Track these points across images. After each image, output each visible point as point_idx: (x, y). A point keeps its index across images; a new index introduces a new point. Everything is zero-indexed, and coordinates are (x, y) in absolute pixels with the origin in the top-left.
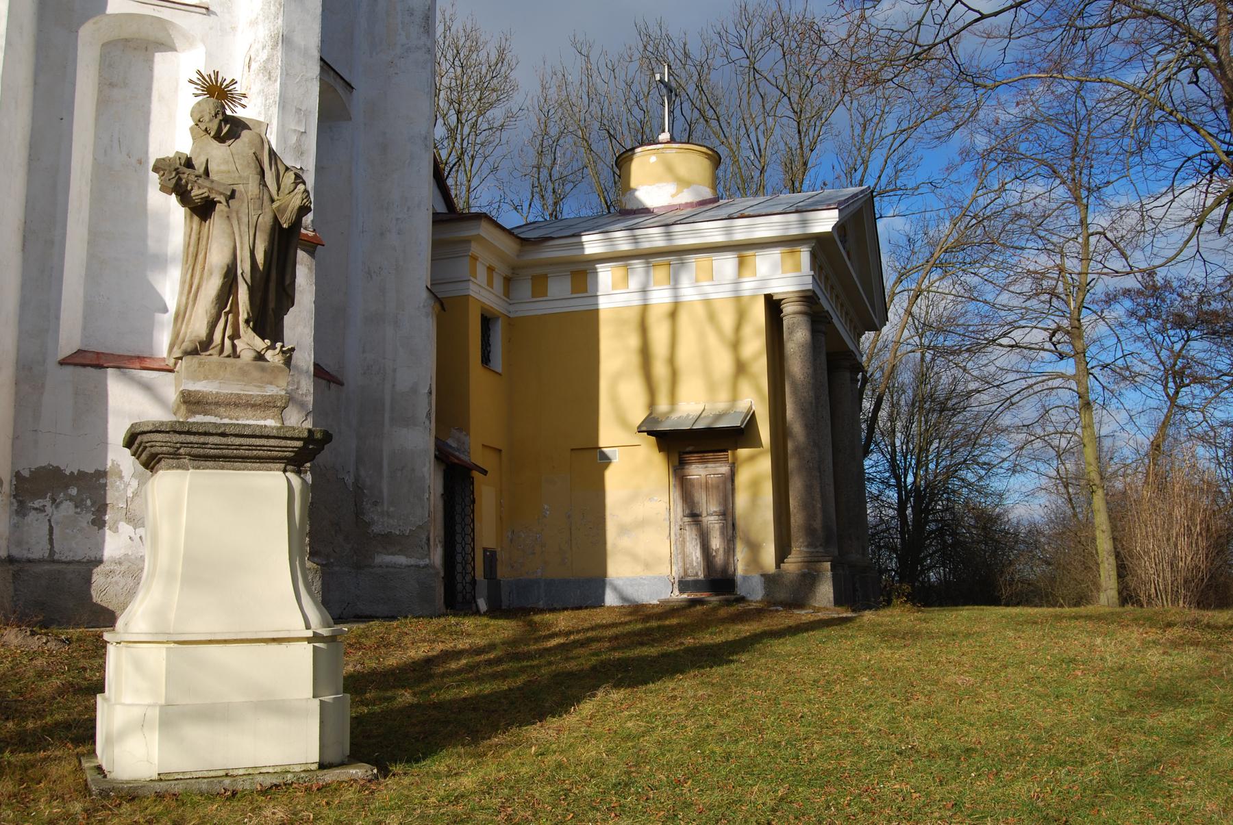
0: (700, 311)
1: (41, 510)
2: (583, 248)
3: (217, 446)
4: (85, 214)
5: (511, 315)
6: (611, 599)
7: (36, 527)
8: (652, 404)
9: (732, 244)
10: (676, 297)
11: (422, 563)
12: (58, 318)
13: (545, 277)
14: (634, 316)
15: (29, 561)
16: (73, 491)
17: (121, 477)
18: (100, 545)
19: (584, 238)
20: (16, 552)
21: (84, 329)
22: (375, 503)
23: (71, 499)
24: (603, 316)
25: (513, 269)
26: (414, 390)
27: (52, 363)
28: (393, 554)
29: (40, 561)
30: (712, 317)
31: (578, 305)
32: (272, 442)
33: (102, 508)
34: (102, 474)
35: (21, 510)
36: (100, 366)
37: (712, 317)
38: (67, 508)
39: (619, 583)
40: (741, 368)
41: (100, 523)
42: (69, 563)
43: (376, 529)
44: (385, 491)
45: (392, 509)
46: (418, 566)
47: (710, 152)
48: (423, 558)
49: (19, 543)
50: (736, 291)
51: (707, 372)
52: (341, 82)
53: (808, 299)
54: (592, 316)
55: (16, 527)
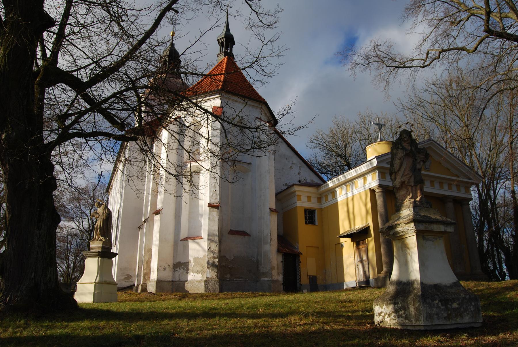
0: (358, 196)
1: (177, 271)
2: (329, 186)
3: (89, 255)
6: (345, 287)
7: (177, 273)
8: (350, 227)
9: (359, 175)
10: (353, 194)
11: (270, 279)
13: (327, 195)
14: (345, 201)
15: (176, 281)
16: (183, 266)
19: (328, 183)
20: (174, 280)
21: (188, 232)
22: (261, 265)
23: (182, 268)
24: (339, 203)
26: (267, 235)
27: (179, 240)
28: (264, 277)
29: (177, 281)
30: (361, 197)
31: (333, 202)
33: (188, 270)
34: (188, 262)
35: (174, 271)
36: (187, 240)
37: (361, 197)
38: (182, 270)
39: (348, 283)
40: (367, 212)
41: (187, 273)
43: (261, 271)
44: (263, 261)
46: (269, 280)
47: (387, 142)
48: (270, 278)
49: (174, 278)
50: (365, 188)
51: (361, 215)
52: (246, 164)
53: (380, 186)
54: (337, 203)
55: (173, 274)
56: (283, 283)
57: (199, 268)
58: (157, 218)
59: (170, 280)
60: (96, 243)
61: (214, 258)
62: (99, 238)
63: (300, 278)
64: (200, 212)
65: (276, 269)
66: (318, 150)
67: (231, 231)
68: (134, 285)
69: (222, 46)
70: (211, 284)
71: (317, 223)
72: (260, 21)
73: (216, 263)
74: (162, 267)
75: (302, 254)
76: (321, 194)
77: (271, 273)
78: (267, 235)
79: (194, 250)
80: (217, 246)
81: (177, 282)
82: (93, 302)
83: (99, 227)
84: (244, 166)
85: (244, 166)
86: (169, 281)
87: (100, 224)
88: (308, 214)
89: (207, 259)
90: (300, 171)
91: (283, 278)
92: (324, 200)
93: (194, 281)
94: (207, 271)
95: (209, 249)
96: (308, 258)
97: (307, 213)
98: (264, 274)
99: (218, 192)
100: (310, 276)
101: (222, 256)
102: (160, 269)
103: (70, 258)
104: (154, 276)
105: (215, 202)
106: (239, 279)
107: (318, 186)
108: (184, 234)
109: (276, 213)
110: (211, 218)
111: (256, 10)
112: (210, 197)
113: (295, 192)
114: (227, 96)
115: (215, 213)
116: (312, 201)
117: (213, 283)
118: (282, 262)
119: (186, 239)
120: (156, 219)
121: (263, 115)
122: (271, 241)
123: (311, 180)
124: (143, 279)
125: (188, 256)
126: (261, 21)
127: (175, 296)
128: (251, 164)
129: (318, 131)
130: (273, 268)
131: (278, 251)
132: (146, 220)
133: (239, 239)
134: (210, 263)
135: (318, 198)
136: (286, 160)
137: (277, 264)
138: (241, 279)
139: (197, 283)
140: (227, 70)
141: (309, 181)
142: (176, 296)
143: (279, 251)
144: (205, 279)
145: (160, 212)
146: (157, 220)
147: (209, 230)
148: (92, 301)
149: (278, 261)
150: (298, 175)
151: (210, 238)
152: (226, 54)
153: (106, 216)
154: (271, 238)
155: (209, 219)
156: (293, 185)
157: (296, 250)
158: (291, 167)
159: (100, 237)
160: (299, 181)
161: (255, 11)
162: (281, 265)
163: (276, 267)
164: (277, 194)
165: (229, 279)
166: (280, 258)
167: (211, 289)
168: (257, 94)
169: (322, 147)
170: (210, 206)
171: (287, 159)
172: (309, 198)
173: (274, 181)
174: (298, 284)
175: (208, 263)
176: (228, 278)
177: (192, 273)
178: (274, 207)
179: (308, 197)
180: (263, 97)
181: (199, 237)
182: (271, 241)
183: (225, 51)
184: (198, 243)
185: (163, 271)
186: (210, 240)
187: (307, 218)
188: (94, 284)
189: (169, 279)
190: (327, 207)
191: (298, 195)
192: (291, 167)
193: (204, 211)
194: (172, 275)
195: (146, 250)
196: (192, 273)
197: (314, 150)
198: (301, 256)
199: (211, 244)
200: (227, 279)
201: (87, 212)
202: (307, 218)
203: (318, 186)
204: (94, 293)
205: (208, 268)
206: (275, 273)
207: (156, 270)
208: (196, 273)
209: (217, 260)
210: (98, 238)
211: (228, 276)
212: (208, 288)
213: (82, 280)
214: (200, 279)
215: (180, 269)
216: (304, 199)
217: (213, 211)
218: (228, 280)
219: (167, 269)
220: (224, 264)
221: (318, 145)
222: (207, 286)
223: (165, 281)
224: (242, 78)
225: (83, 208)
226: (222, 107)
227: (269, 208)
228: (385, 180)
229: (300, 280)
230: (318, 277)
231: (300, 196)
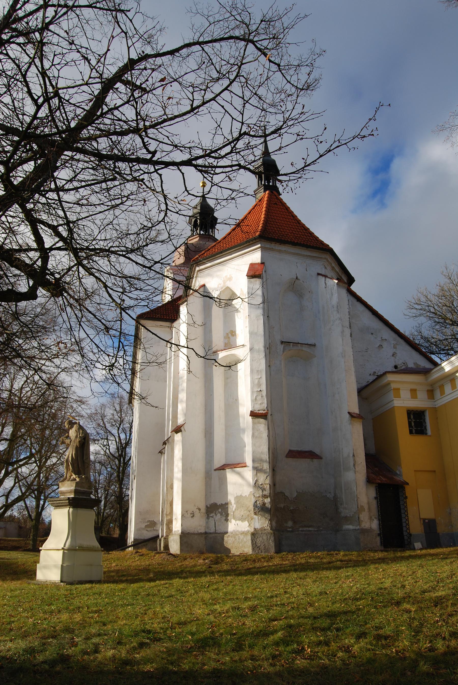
1: (212, 517)
2: (444, 370)
4: (223, 421)
5: (437, 406)
7: (211, 521)
12: (213, 456)
15: (210, 533)
16: (220, 510)
17: (231, 504)
18: (227, 527)
19: (443, 365)
20: (208, 531)
21: (226, 457)
22: (341, 504)
23: (219, 513)
25: (431, 385)
26: (349, 456)
28: (348, 525)
32: (64, 501)
33: (227, 515)
34: (227, 504)
35: (208, 517)
36: (224, 469)
41: (227, 520)
42: (219, 533)
43: (343, 515)
45: (346, 506)
46: (356, 530)
48: (357, 526)
52: (306, 346)
55: (207, 523)
56: (379, 532)
57: (243, 512)
58: (178, 437)
59: (203, 531)
60: (66, 485)
61: (265, 496)
62: (72, 477)
63: (408, 524)
64: (241, 425)
66: (422, 319)
67: (290, 451)
68: (158, 536)
69: (260, 179)
70: (261, 539)
71: (429, 432)
72: (288, 81)
73: (268, 505)
74: (189, 513)
75: (408, 484)
76: (432, 385)
77: (359, 518)
78: (349, 456)
79: (235, 484)
80: (268, 478)
81: (214, 535)
82: (61, 581)
83: (70, 459)
84: (304, 349)
85: (304, 349)
86: (201, 534)
87: (72, 455)
88: (414, 418)
89: (253, 500)
90: (394, 350)
91: (379, 525)
92: (437, 394)
93: (238, 533)
94: (255, 518)
95: (255, 484)
96: (418, 490)
97: (412, 417)
98: (347, 519)
99: (264, 393)
100: (424, 520)
101: (278, 492)
102: (186, 515)
103: (99, 491)
104: (177, 527)
105: (261, 408)
106: (307, 529)
107: (426, 372)
108: (218, 461)
109: (362, 420)
110: (256, 434)
111: (277, 62)
112: (252, 401)
113: (388, 384)
114: (268, 245)
115: (262, 425)
117: (265, 537)
118: (376, 498)
119: (223, 468)
120: (177, 439)
121: (329, 268)
122: (354, 465)
123: (414, 364)
124: (166, 529)
125: (226, 494)
126: (290, 83)
127: (204, 560)
128: (314, 345)
129: (419, 290)
130: (360, 509)
131: (367, 481)
132: (166, 442)
133: (304, 463)
134: (259, 505)
136: (370, 335)
137: (368, 503)
138: (310, 529)
139: (242, 537)
140: (268, 209)
141: (411, 365)
142: (207, 561)
143: (369, 481)
144: (252, 530)
145: (182, 429)
146: (178, 441)
147: (253, 452)
148: (59, 579)
149: (368, 498)
150: (393, 358)
151: (256, 465)
152: (266, 188)
153: (79, 441)
154: (354, 460)
155: (253, 436)
156: (385, 373)
157: (397, 478)
158: (381, 346)
159: (73, 474)
160: (396, 367)
161: (258, 27)
162: (374, 504)
163: (366, 507)
164: (360, 391)
165: (291, 530)
166: (372, 492)
167: (262, 547)
168: (317, 238)
169: (428, 314)
170: (253, 414)
171: (372, 334)
172: (413, 392)
173: (353, 369)
174: (405, 533)
175: (255, 506)
176: (290, 528)
177: (233, 521)
178: (356, 410)
179: (411, 390)
180: (326, 242)
181: (242, 463)
182: (354, 465)
183: (264, 185)
184: (239, 474)
185: (191, 518)
186: (257, 470)
187: (413, 424)
188: (62, 551)
189: (200, 529)
190: (445, 404)
192: (381, 346)
193: (247, 423)
194: (205, 525)
195: (169, 486)
196: (233, 521)
197: (416, 319)
198: (407, 488)
199: (258, 474)
200: (288, 530)
201: (115, 431)
202: (413, 424)
203: (426, 372)
204: (62, 566)
205: (255, 513)
206: (364, 516)
207: (180, 517)
208: (239, 520)
209: (269, 500)
210: (70, 477)
211: (290, 524)
212: (256, 546)
213: (47, 545)
214: (246, 529)
215: (216, 515)
216: (405, 394)
217: (259, 423)
219: (197, 514)
220: (282, 506)
221: (421, 312)
222: (256, 542)
223: (194, 534)
224: (292, 218)
225: (108, 426)
226: (262, 263)
227: (349, 413)
229: (408, 527)
230: (437, 521)
231: (398, 389)
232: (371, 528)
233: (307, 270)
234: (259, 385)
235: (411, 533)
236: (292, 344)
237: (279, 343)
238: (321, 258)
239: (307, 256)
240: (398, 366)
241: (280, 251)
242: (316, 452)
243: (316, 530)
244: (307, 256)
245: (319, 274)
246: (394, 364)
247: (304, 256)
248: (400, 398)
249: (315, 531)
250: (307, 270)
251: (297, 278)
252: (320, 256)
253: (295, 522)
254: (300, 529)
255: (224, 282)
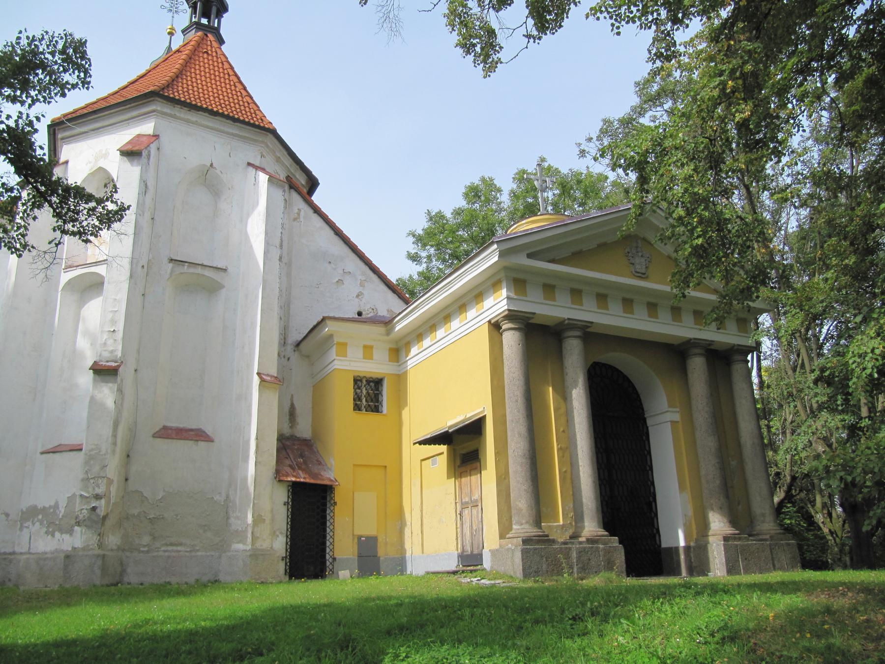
1: (27, 527)
15: (21, 553)
16: (40, 517)
23: (38, 520)
43: (233, 528)
65: (268, 521)
67: (165, 428)
81: (25, 557)
90: (361, 289)
99: (120, 335)
100: (359, 537)
106: (175, 548)
113: (331, 337)
116: (375, 356)
123: (388, 311)
128: (225, 270)
135: (391, 350)
138: (179, 548)
150: (357, 300)
165: (146, 549)
171: (330, 262)
172: (368, 351)
176: (144, 546)
179: (365, 347)
191: (339, 344)
192: (340, 282)
200: (141, 549)
211: (146, 540)
215: (34, 524)
218: (143, 552)
220: (135, 512)
228: (525, 298)
232: (272, 548)
233: (230, 156)
234: (113, 322)
235: (335, 556)
236: (186, 264)
237: (166, 260)
238: (256, 141)
239: (232, 134)
240: (364, 313)
241: (187, 121)
242: (206, 431)
243: (188, 550)
244: (232, 134)
245: (249, 164)
246: (358, 310)
247: (228, 133)
248: (372, 359)
249: (187, 552)
250: (230, 156)
251: (212, 165)
252: (255, 138)
253: (154, 538)
254: (163, 549)
255: (96, 161)
